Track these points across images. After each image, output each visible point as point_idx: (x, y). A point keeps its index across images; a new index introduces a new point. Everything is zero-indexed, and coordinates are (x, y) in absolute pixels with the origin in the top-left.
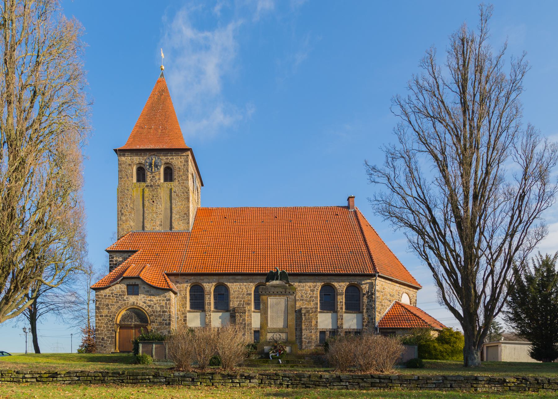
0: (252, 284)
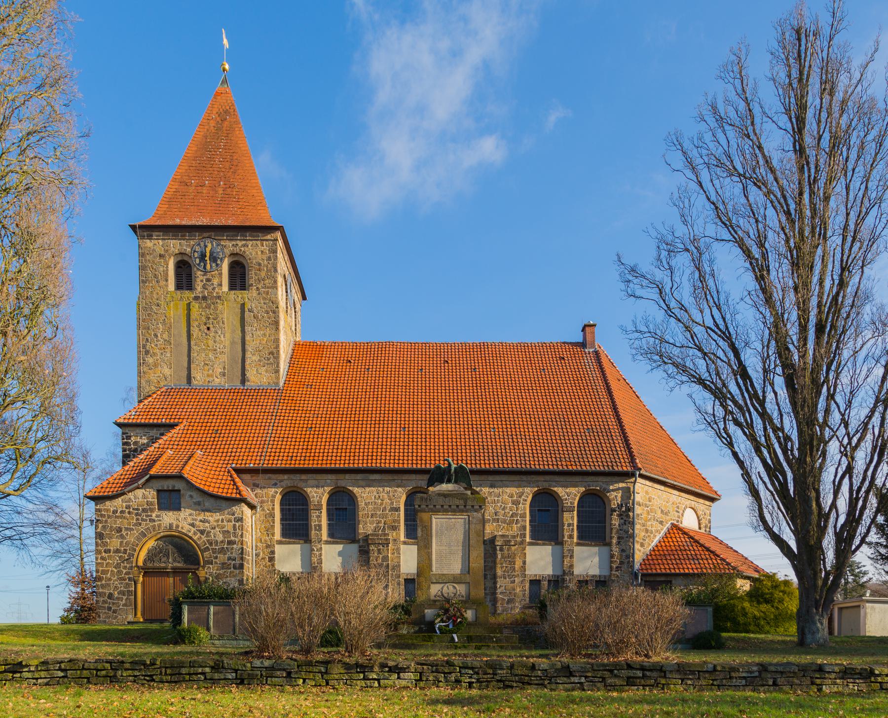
0: (400, 489)
